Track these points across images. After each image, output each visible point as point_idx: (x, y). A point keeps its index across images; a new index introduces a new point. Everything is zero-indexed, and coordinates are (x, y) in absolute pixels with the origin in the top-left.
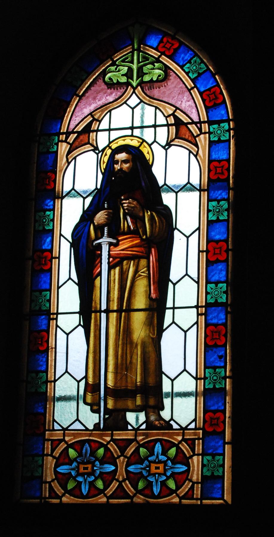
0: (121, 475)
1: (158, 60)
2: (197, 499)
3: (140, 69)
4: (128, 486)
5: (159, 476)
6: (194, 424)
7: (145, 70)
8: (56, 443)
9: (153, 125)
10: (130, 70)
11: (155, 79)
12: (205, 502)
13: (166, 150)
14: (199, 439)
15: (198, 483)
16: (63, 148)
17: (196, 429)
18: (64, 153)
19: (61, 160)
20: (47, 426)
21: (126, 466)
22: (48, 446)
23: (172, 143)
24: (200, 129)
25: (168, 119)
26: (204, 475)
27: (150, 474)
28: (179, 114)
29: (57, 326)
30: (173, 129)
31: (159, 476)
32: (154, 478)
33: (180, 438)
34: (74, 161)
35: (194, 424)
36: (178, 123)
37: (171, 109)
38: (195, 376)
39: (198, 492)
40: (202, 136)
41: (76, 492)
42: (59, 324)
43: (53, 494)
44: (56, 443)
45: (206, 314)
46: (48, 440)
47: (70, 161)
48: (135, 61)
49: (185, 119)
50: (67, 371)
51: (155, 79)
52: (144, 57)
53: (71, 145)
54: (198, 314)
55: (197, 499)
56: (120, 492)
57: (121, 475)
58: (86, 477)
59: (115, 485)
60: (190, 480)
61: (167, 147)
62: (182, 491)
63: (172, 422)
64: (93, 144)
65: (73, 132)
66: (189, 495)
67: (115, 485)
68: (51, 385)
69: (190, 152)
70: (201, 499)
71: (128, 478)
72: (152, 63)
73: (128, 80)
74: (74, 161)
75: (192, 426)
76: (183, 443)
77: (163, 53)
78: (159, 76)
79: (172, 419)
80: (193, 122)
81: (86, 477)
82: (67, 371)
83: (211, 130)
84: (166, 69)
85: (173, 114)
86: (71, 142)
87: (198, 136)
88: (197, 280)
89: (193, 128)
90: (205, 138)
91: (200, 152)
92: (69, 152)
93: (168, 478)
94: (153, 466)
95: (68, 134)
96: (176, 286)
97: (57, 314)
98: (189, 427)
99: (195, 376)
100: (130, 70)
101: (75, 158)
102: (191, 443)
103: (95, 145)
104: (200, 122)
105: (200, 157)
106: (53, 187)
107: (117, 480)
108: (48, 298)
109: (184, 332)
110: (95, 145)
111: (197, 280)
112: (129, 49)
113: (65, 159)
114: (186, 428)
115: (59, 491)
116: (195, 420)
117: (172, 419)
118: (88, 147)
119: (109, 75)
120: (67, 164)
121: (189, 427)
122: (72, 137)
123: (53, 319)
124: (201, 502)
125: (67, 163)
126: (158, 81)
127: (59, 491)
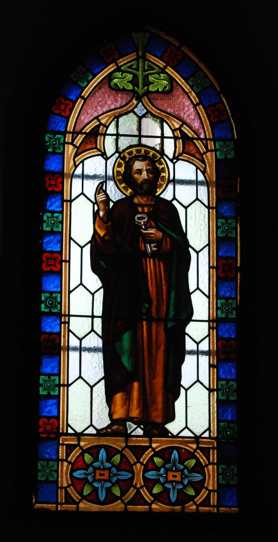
0: (139, 481)
1: (163, 71)
2: (213, 506)
3: (146, 78)
4: (144, 492)
5: (100, 467)
6: (208, 432)
7: (151, 78)
8: (70, 448)
9: (161, 140)
10: (135, 77)
11: (160, 90)
12: (222, 509)
13: (174, 164)
14: (213, 448)
15: (214, 491)
16: (70, 150)
17: (210, 437)
18: (71, 155)
19: (69, 163)
20: (216, 496)
21: (143, 472)
22: (62, 452)
23: (180, 157)
24: (206, 147)
25: (175, 132)
26: (84, 495)
27: (109, 469)
28: (186, 129)
29: (69, 331)
30: (180, 142)
31: (100, 467)
32: (100, 484)
33: (194, 446)
34: (81, 164)
35: (208, 432)
36: (184, 137)
37: (178, 123)
38: (208, 387)
39: (214, 499)
40: (209, 154)
41: (93, 498)
42: (71, 328)
43: (69, 500)
44: (70, 448)
45: (216, 328)
46: (63, 445)
47: (77, 164)
48: (141, 69)
49: (191, 134)
50: (92, 387)
51: (160, 90)
52: (149, 66)
53: (78, 148)
54: (210, 328)
55: (213, 506)
56: (138, 499)
57: (139, 481)
58: (174, 484)
59: (132, 492)
60: (69, 463)
61: (175, 161)
62: (199, 499)
63: (175, 203)
64: (101, 150)
65: (80, 132)
66: (206, 502)
67: (132, 492)
68: (64, 390)
69: (197, 168)
70: (218, 506)
71: (72, 484)
72: (158, 73)
73: (133, 88)
74: (81, 164)
75: (206, 435)
76: (198, 451)
77: (168, 64)
78: (165, 87)
79: (174, 198)
80: (199, 139)
81: (174, 484)
82: (92, 387)
83: (217, 147)
84: (171, 79)
85: (179, 129)
86: (78, 145)
87: (205, 153)
88: (208, 295)
89: (199, 144)
90: (212, 155)
91: (208, 169)
92: (76, 156)
93: (113, 485)
94: (178, 479)
95: (75, 134)
96: (188, 392)
97: (69, 316)
98: (203, 436)
99: (208, 387)
100: (135, 77)
101: (83, 162)
102: (206, 452)
103: (103, 151)
104: (206, 139)
105: (208, 174)
106: (61, 189)
107: (135, 487)
108: (59, 300)
109: (199, 288)
110: (103, 151)
111: (208, 295)
112: (133, 56)
113: (72, 163)
114: (200, 437)
115: (75, 496)
116: (209, 429)
117: (174, 198)
118: (95, 152)
119: (115, 81)
120: (74, 168)
121: (203, 436)
122: (79, 140)
123: (65, 323)
124: (218, 510)
125: (74, 167)
126: (163, 92)
127: (75, 496)
